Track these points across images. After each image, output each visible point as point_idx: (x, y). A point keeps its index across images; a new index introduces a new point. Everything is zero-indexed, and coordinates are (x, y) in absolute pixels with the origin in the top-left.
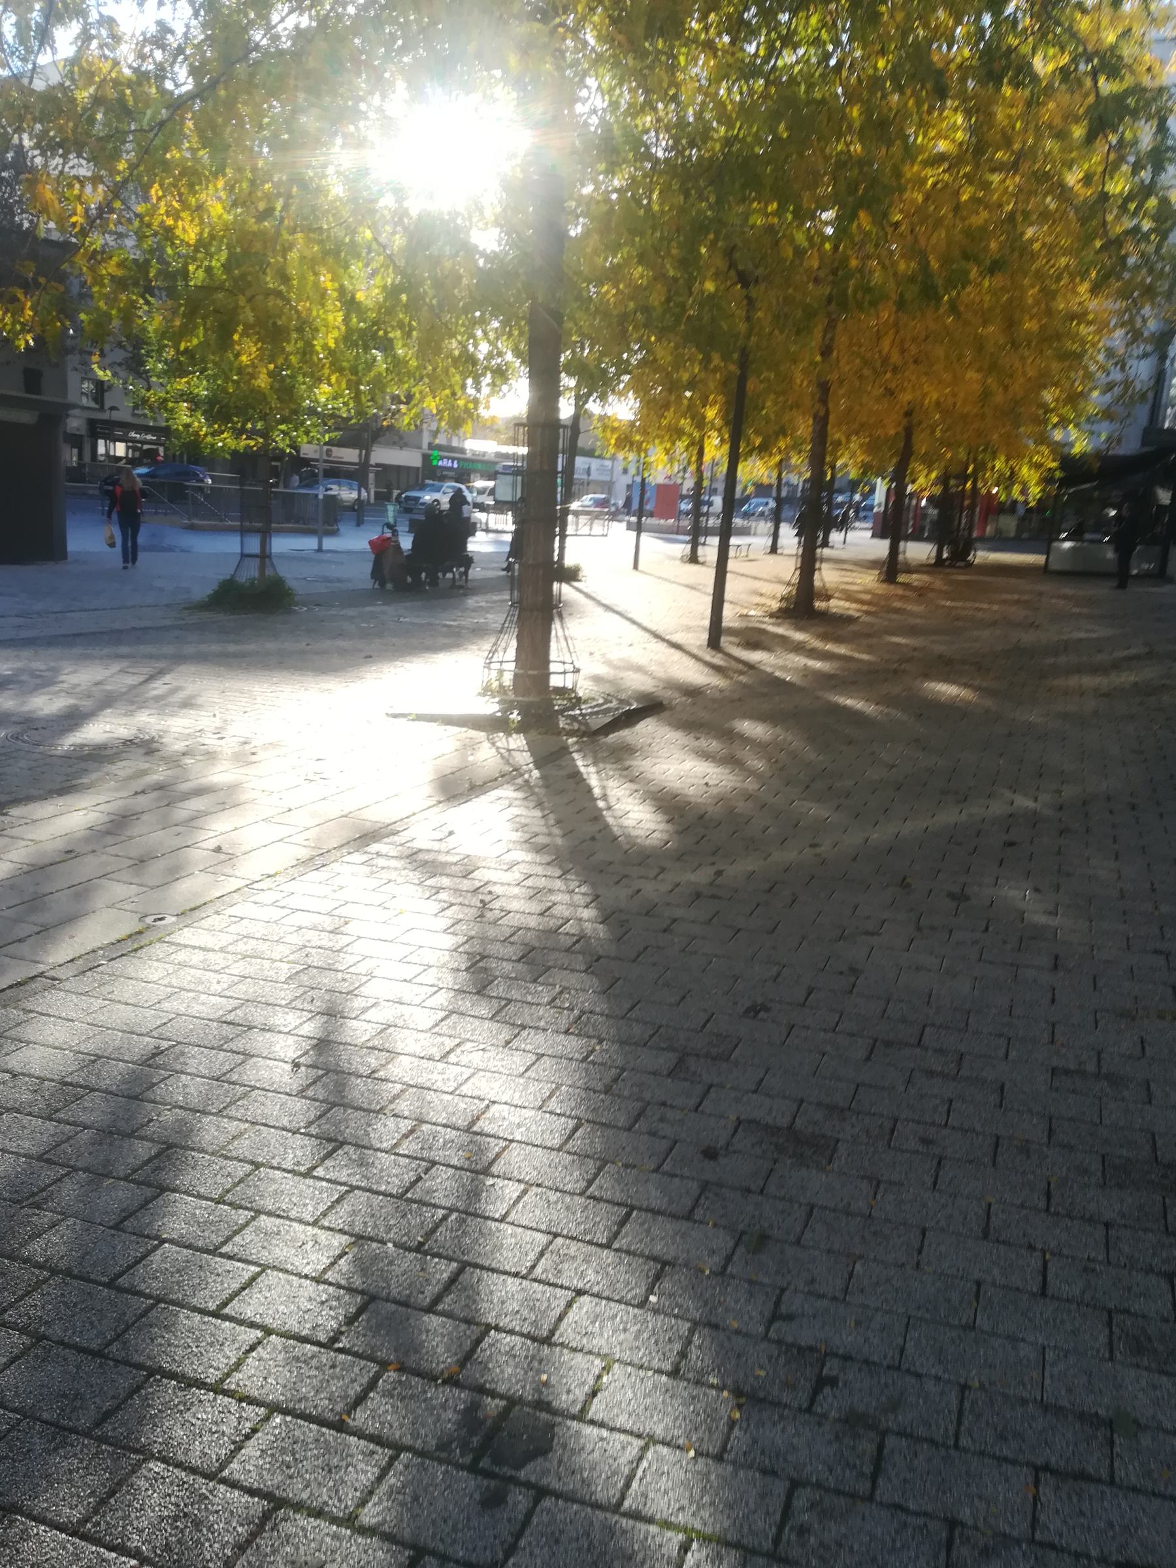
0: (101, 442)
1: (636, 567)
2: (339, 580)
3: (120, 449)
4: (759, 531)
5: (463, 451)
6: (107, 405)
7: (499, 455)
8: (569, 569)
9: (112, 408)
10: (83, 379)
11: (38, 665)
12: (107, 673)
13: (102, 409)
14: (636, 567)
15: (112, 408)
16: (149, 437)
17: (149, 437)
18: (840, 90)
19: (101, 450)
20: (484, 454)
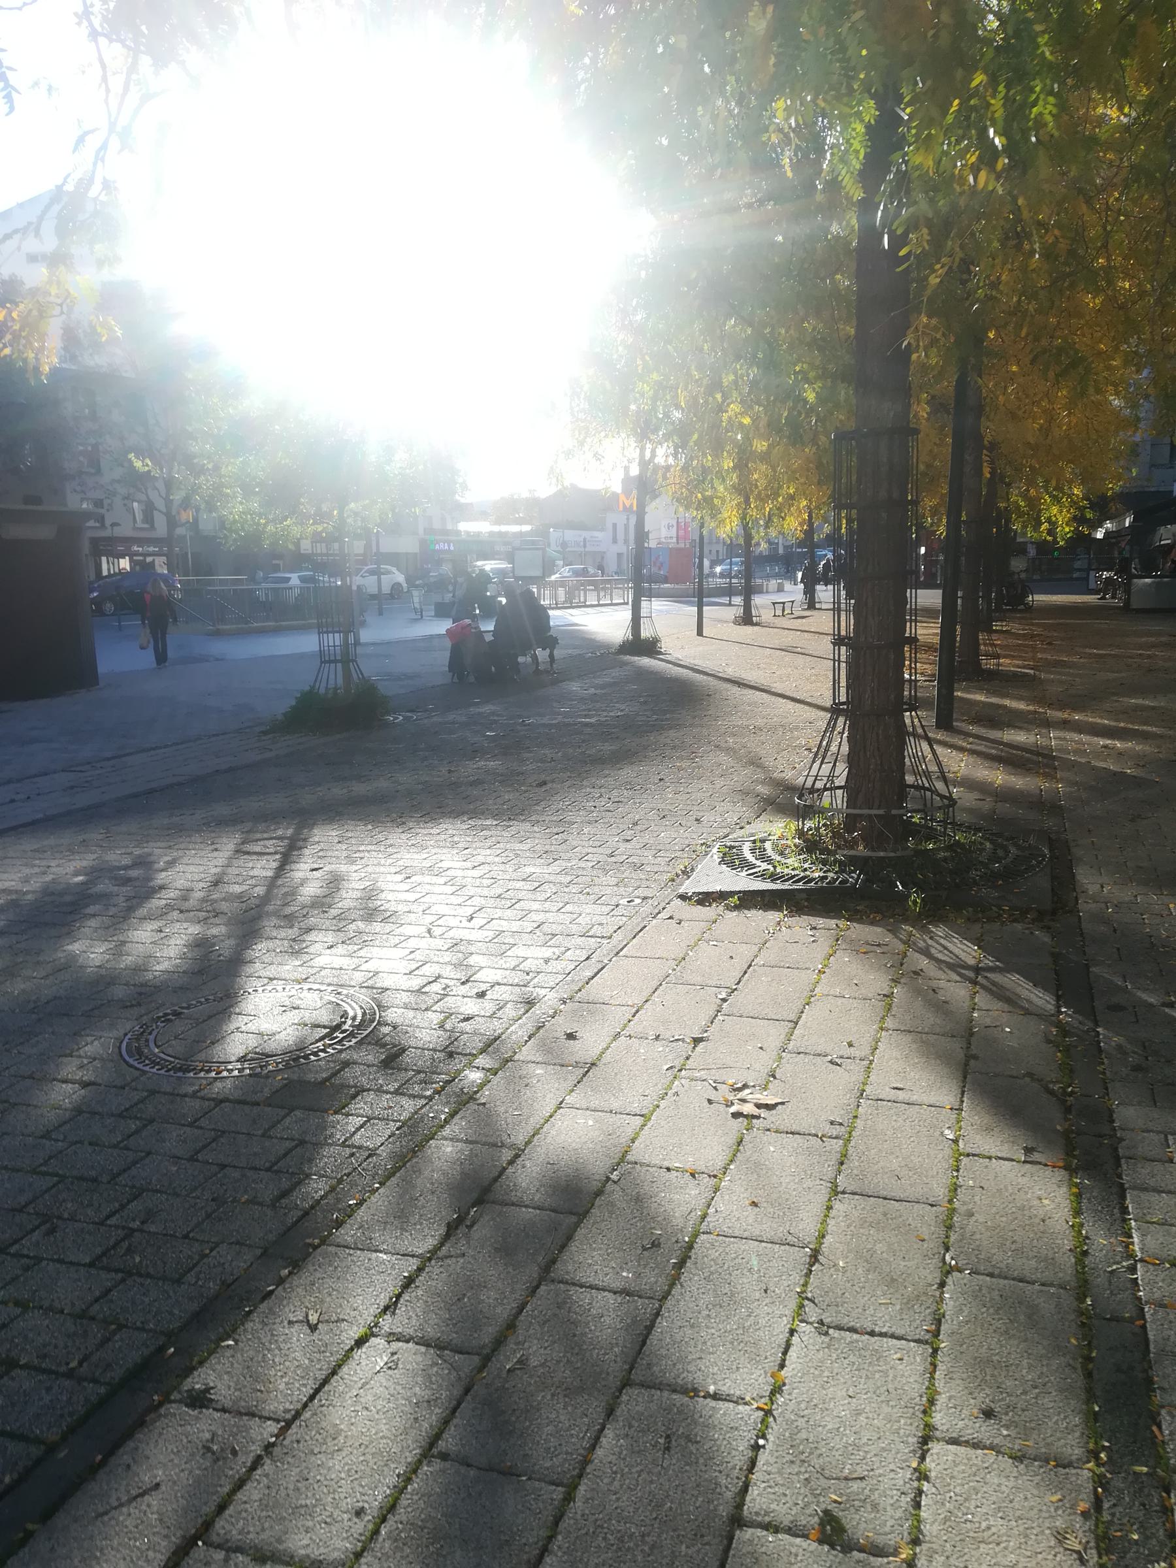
0: (104, 559)
1: (700, 633)
2: (577, 625)
3: (125, 564)
4: (771, 588)
5: (458, 533)
6: (108, 523)
7: (491, 534)
8: (647, 640)
9: (113, 525)
10: (82, 500)
11: (117, 857)
12: (221, 858)
13: (103, 526)
14: (700, 633)
15: (113, 525)
16: (151, 549)
17: (151, 549)
18: (785, 414)
19: (105, 566)
20: (479, 534)
